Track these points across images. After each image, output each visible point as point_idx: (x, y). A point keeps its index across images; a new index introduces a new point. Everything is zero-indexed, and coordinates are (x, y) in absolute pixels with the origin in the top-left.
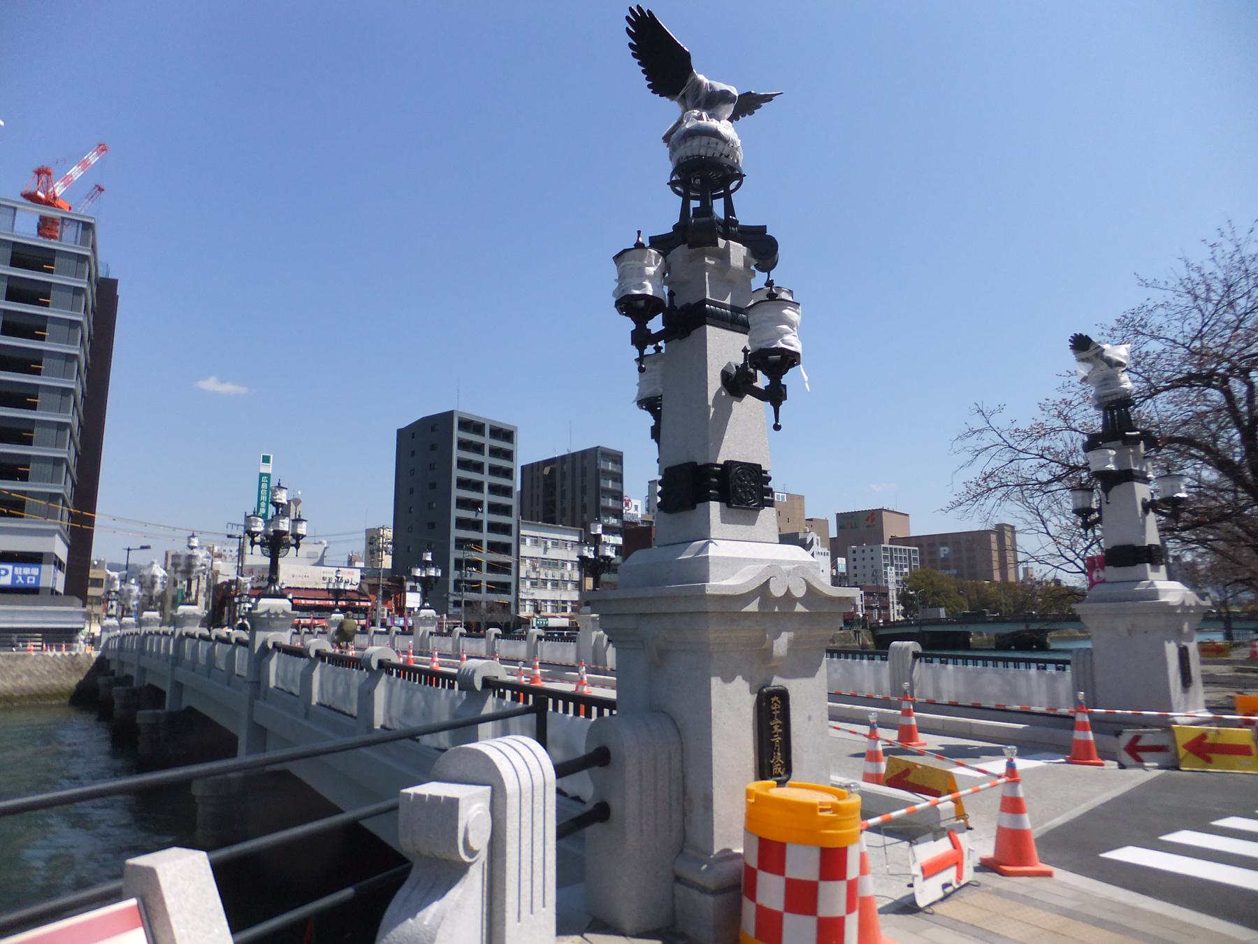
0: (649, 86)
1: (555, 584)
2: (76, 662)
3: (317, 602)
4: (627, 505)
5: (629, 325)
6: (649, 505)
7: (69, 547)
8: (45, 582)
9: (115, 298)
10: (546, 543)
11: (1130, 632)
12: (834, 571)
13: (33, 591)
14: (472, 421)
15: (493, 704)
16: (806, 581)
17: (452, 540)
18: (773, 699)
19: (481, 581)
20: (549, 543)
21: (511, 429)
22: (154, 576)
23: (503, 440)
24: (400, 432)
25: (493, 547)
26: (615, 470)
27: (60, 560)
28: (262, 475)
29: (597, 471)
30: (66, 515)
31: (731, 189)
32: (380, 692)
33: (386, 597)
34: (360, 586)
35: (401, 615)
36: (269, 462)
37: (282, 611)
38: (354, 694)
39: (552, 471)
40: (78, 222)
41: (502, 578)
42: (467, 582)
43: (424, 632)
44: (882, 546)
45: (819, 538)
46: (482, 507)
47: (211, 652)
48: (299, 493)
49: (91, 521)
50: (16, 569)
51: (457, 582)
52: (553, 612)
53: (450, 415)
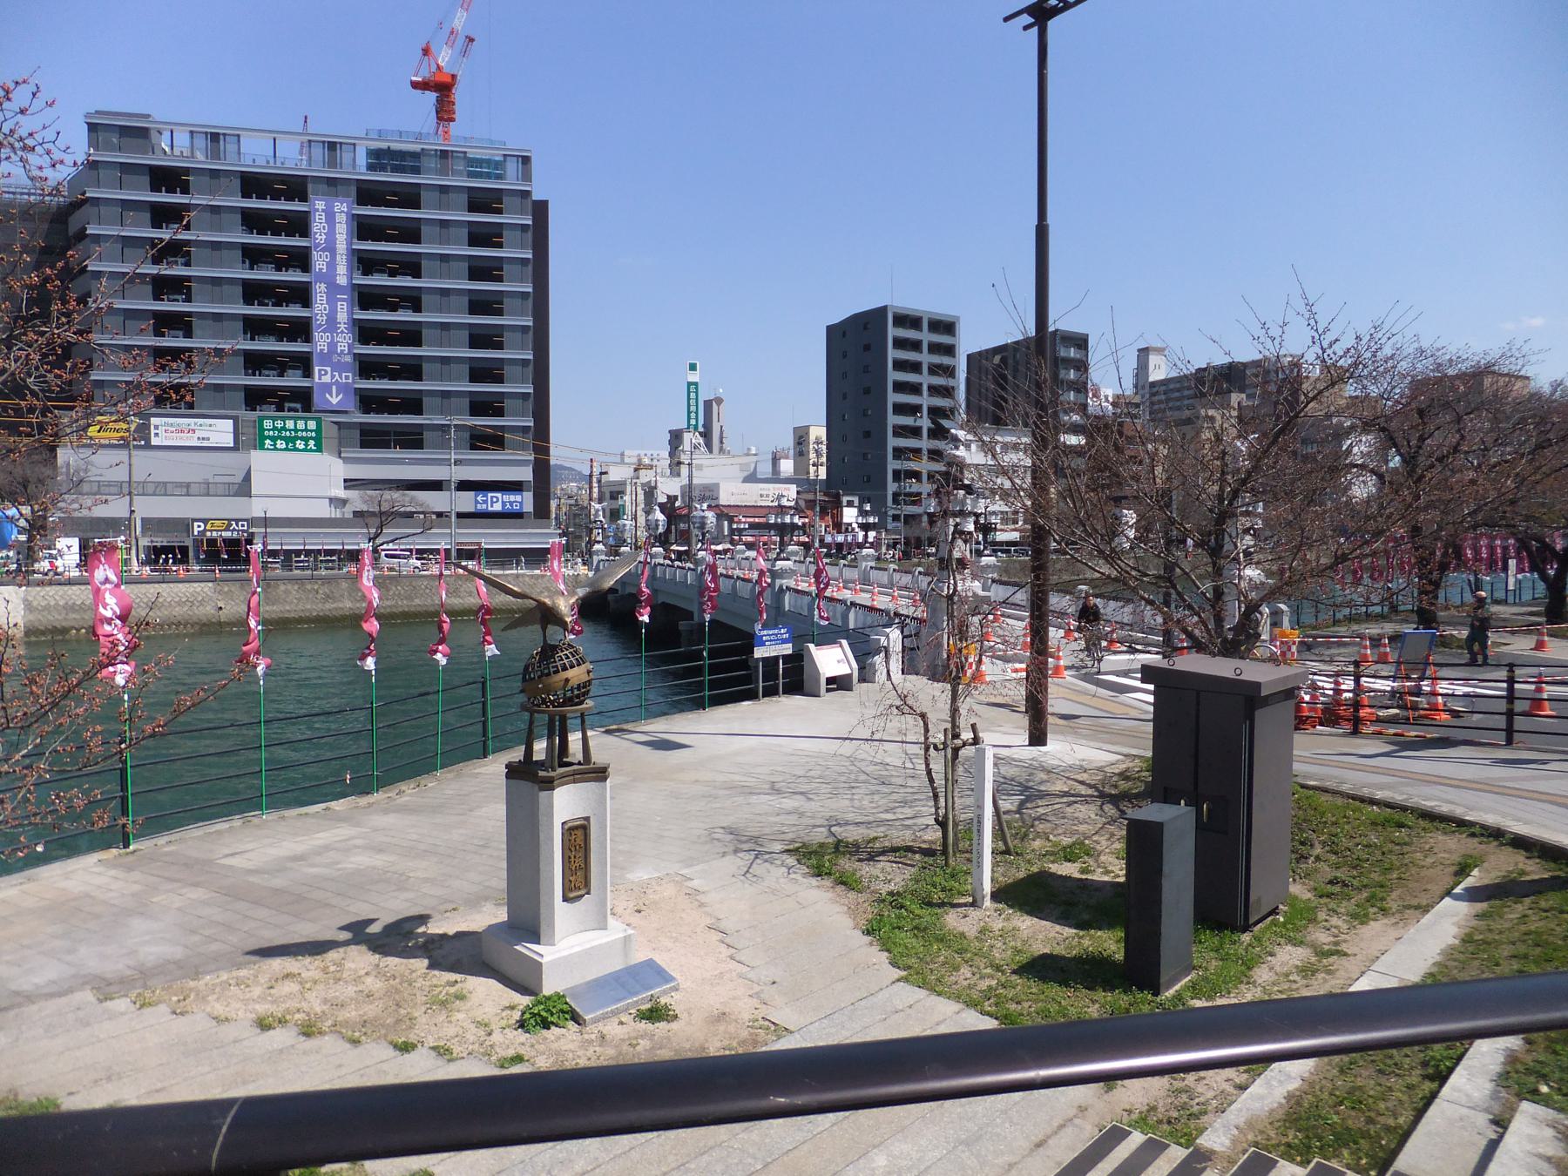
3: (757, 520)
6: (1137, 380)
14: (908, 315)
19: (921, 494)
22: (657, 520)
24: (830, 329)
26: (1078, 356)
28: (690, 384)
32: (852, 616)
33: (823, 513)
34: (797, 503)
35: (839, 532)
38: (839, 616)
39: (1004, 360)
42: (906, 495)
43: (866, 566)
46: (921, 412)
47: (734, 587)
51: (896, 495)
53: (883, 310)
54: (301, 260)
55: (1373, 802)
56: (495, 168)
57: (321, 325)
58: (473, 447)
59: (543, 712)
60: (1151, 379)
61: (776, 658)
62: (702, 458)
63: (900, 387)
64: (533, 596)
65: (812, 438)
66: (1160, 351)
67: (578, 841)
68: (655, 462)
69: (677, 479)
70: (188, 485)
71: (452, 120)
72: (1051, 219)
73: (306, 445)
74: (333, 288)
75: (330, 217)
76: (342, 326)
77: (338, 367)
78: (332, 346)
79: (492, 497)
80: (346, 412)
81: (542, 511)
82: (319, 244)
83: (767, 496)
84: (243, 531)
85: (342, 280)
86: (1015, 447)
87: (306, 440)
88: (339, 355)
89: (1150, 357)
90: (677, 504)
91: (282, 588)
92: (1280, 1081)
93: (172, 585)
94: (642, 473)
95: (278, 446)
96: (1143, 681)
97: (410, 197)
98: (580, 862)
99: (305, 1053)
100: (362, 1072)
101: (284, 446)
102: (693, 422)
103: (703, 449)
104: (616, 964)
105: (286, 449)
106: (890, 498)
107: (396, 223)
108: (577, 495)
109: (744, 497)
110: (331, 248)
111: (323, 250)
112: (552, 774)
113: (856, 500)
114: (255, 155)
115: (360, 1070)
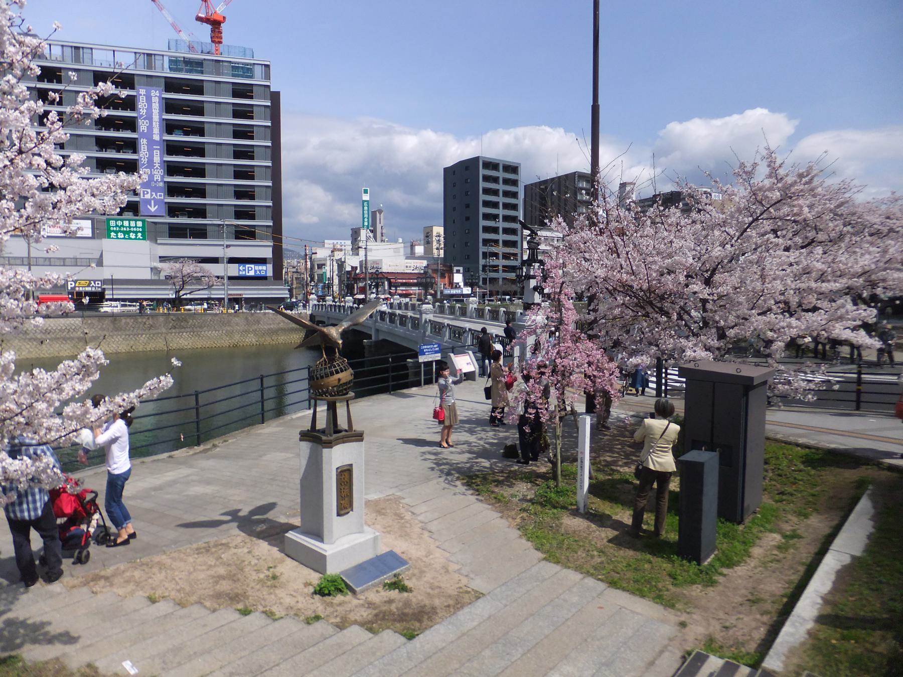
13: (264, 278)
17: (481, 241)
25: (506, 243)
40: (262, 65)
41: (512, 176)
42: (490, 266)
53: (477, 159)
54: (131, 124)
55: (798, 445)
56: (247, 70)
57: (144, 164)
58: (237, 238)
59: (324, 400)
61: (432, 362)
62: (372, 244)
63: (486, 204)
65: (435, 234)
67: (346, 479)
68: (343, 247)
69: (357, 257)
70: (64, 259)
71: (220, 42)
72: (600, 102)
73: (136, 236)
74: (151, 142)
75: (149, 99)
76: (157, 165)
77: (155, 189)
78: (151, 177)
80: (162, 216)
81: (278, 274)
82: (142, 115)
83: (410, 267)
84: (98, 287)
85: (156, 137)
87: (136, 233)
88: (155, 182)
90: (358, 271)
91: (124, 321)
92: (800, 623)
93: (56, 320)
94: (336, 253)
95: (119, 237)
96: (679, 376)
97: (197, 88)
98: (347, 491)
99: (181, 617)
100: (219, 629)
101: (123, 236)
102: (366, 224)
103: (372, 239)
104: (368, 555)
105: (124, 238)
106: (481, 268)
107: (189, 104)
108: (297, 266)
109: (397, 268)
110: (149, 117)
111: (145, 119)
112: (331, 438)
113: (461, 269)
114: (101, 61)
115: (218, 628)
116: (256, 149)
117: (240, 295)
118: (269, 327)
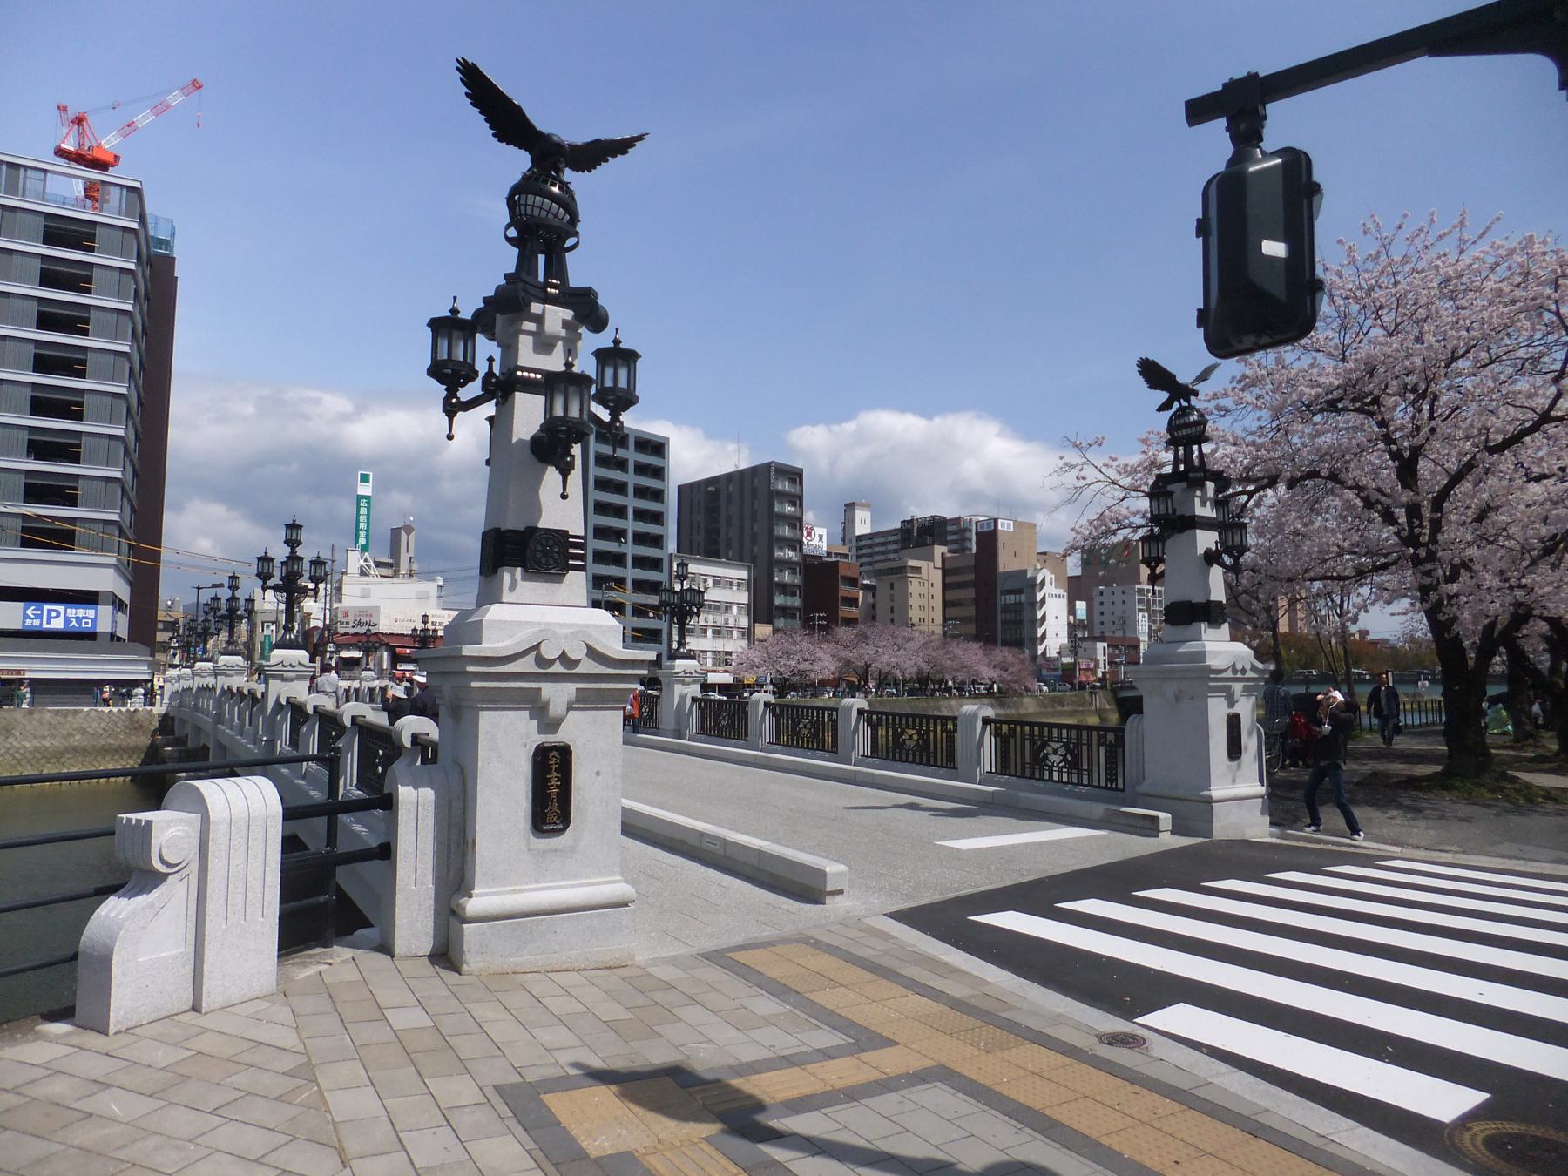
0: (494, 135)
1: (717, 632)
2: (136, 719)
4: (809, 534)
5: (440, 390)
7: (131, 584)
8: (104, 626)
9: (173, 281)
10: (705, 581)
11: (1177, 698)
12: (1071, 618)
13: (90, 636)
14: (648, 533)
15: (1414, 819)
16: (587, 645)
18: (551, 755)
20: (710, 582)
21: (662, 441)
23: (651, 455)
26: (792, 490)
27: (120, 600)
28: (360, 497)
29: (771, 492)
30: (125, 548)
31: (566, 246)
36: (368, 482)
37: (557, 654)
40: (122, 186)
44: (1137, 586)
45: (1053, 576)
46: (625, 537)
48: (412, 518)
49: (156, 556)
50: (69, 610)
52: (713, 665)
58: (26, 543)
60: (857, 533)
64: (926, 814)
66: (865, 506)
79: (49, 611)
86: (728, 583)
89: (857, 512)
116: (90, 356)
117: (18, 672)
118: (36, 743)
